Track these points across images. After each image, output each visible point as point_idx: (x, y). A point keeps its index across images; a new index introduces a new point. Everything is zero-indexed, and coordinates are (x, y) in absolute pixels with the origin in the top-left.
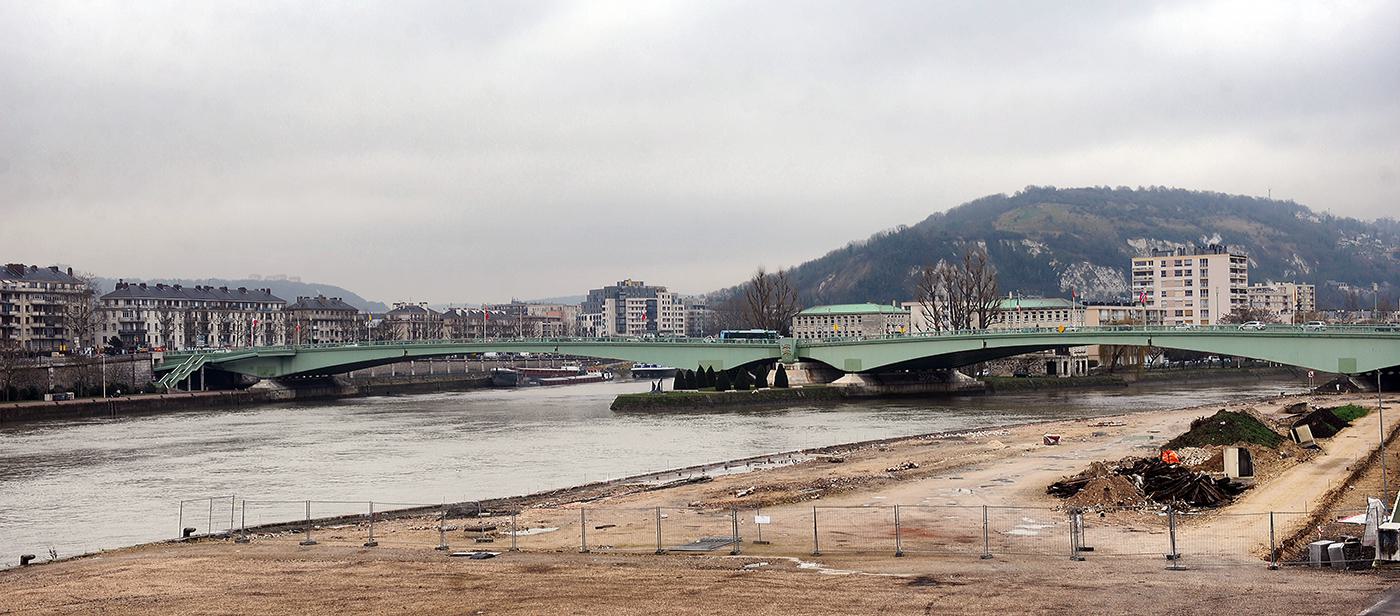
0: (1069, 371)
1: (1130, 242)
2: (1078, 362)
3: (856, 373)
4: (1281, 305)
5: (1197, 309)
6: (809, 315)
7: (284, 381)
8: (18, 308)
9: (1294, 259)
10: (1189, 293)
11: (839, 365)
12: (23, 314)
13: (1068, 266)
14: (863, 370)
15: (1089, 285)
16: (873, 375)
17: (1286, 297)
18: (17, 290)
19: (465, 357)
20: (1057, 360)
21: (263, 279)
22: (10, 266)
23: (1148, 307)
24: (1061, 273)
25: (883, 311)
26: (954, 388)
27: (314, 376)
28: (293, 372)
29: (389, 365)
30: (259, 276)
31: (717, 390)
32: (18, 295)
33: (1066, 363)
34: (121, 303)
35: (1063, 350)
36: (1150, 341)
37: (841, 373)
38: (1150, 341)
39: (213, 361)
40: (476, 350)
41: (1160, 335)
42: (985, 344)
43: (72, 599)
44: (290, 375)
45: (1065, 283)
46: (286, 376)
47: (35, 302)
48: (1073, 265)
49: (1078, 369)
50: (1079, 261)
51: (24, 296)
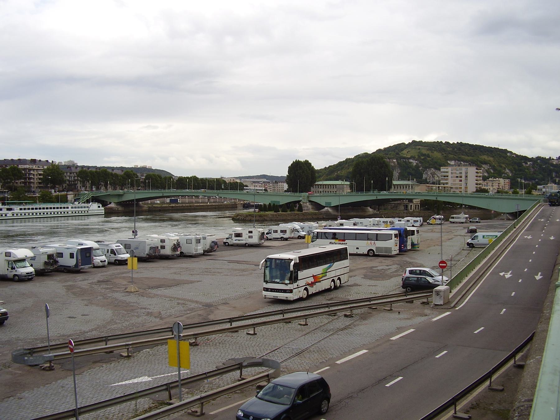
0: (412, 209)
1: (449, 162)
2: (416, 205)
3: (329, 207)
4: (497, 186)
5: (463, 187)
6: (319, 184)
7: (118, 204)
8: (34, 175)
9: (506, 170)
10: (461, 181)
11: (323, 204)
12: (532, 169)
13: (426, 170)
14: (332, 206)
15: (433, 177)
16: (336, 208)
17: (499, 184)
18: (33, 168)
19: (187, 197)
20: (408, 205)
21: (139, 167)
22: (32, 159)
23: (445, 186)
24: (423, 172)
25: (345, 184)
26: (368, 213)
27: (129, 202)
28: (121, 201)
29: (164, 198)
30: (137, 166)
31: (275, 212)
32: (34, 170)
33: (411, 206)
34: (68, 174)
35: (411, 201)
36: (437, 198)
37: (324, 207)
38: (437, 198)
39: (95, 195)
40: (197, 195)
41: (440, 196)
42: (377, 197)
43: (351, 327)
44: (122, 202)
45: (424, 176)
46: (121, 202)
47: (39, 173)
48: (428, 170)
49: (416, 208)
50: (429, 168)
51: (36, 170)
